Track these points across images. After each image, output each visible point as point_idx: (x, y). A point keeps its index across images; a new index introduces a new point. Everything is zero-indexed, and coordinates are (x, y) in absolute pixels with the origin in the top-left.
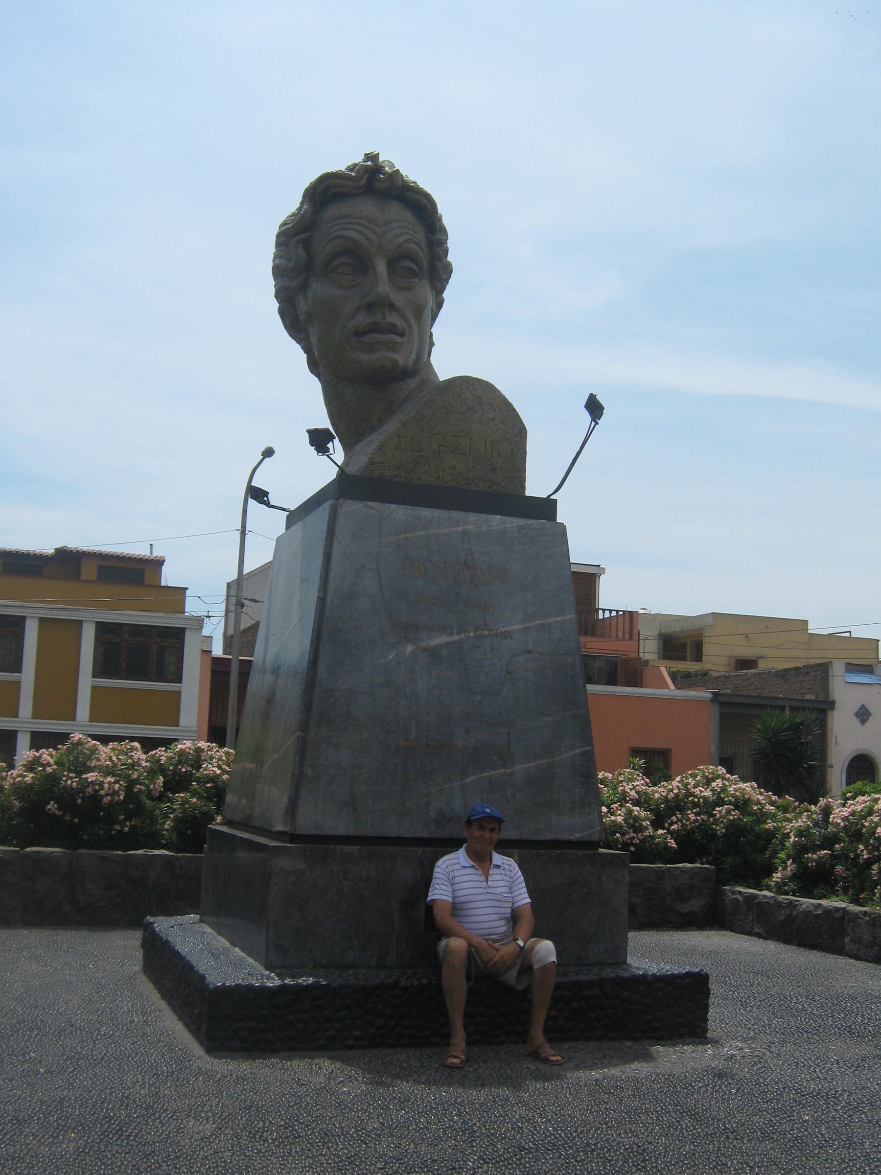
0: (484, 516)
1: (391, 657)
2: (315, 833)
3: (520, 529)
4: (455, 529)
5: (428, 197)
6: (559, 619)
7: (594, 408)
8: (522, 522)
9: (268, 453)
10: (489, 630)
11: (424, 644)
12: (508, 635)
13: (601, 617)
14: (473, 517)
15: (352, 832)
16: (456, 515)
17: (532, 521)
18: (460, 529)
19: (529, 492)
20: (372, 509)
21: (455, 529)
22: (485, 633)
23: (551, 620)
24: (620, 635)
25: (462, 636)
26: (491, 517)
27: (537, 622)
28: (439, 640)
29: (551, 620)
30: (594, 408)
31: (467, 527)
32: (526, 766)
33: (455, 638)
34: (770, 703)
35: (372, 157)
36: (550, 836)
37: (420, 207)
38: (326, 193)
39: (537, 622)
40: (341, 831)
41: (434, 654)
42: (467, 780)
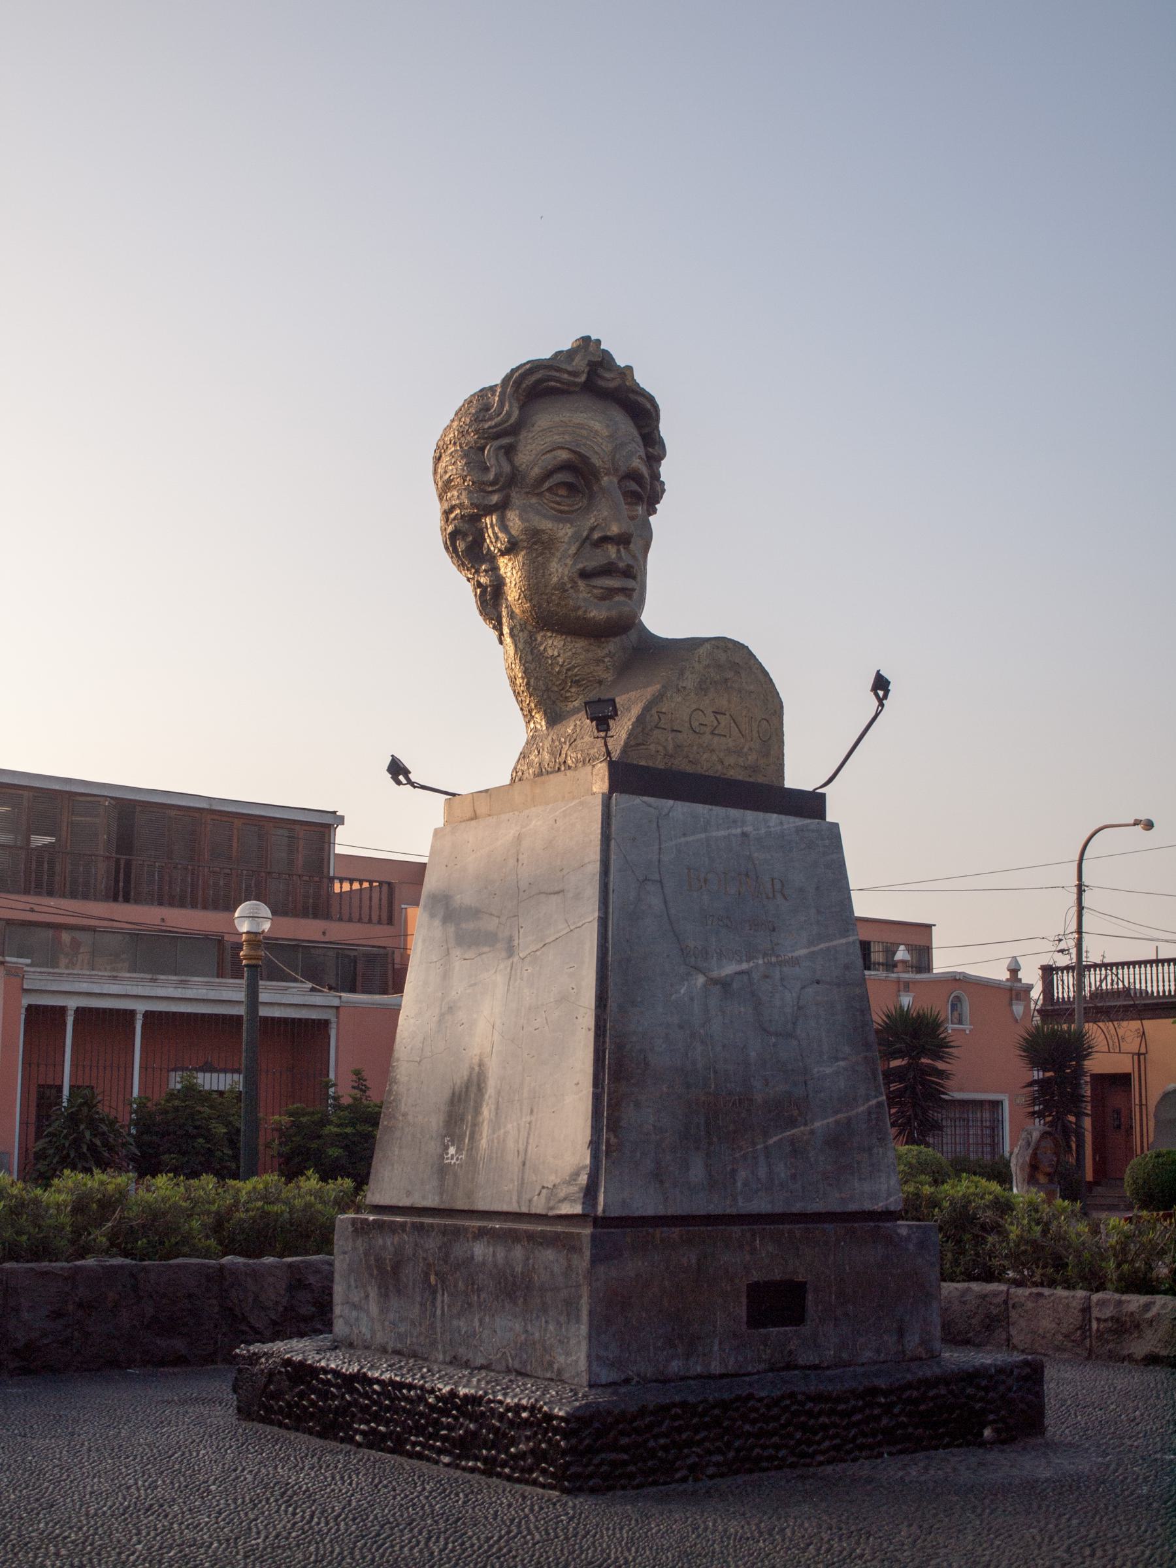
0: (761, 815)
1: (682, 991)
2: (839, 1210)
3: (799, 830)
4: (734, 831)
5: (651, 399)
6: (844, 941)
7: (881, 685)
8: (799, 822)
9: (1149, 825)
10: (778, 956)
11: (715, 974)
12: (795, 962)
13: (337, 889)
14: (750, 815)
15: (661, 1211)
16: (734, 813)
17: (809, 821)
18: (739, 831)
19: (788, 784)
20: (650, 806)
21: (734, 831)
22: (774, 959)
23: (835, 943)
24: (375, 918)
25: (751, 964)
26: (768, 815)
27: (822, 946)
28: (730, 969)
29: (835, 943)
30: (881, 685)
31: (745, 829)
32: (825, 1122)
33: (745, 966)
34: (1064, 1040)
35: (586, 340)
36: (852, 1207)
37: (641, 412)
38: (535, 385)
39: (822, 946)
40: (650, 1212)
41: (725, 985)
42: (771, 1142)
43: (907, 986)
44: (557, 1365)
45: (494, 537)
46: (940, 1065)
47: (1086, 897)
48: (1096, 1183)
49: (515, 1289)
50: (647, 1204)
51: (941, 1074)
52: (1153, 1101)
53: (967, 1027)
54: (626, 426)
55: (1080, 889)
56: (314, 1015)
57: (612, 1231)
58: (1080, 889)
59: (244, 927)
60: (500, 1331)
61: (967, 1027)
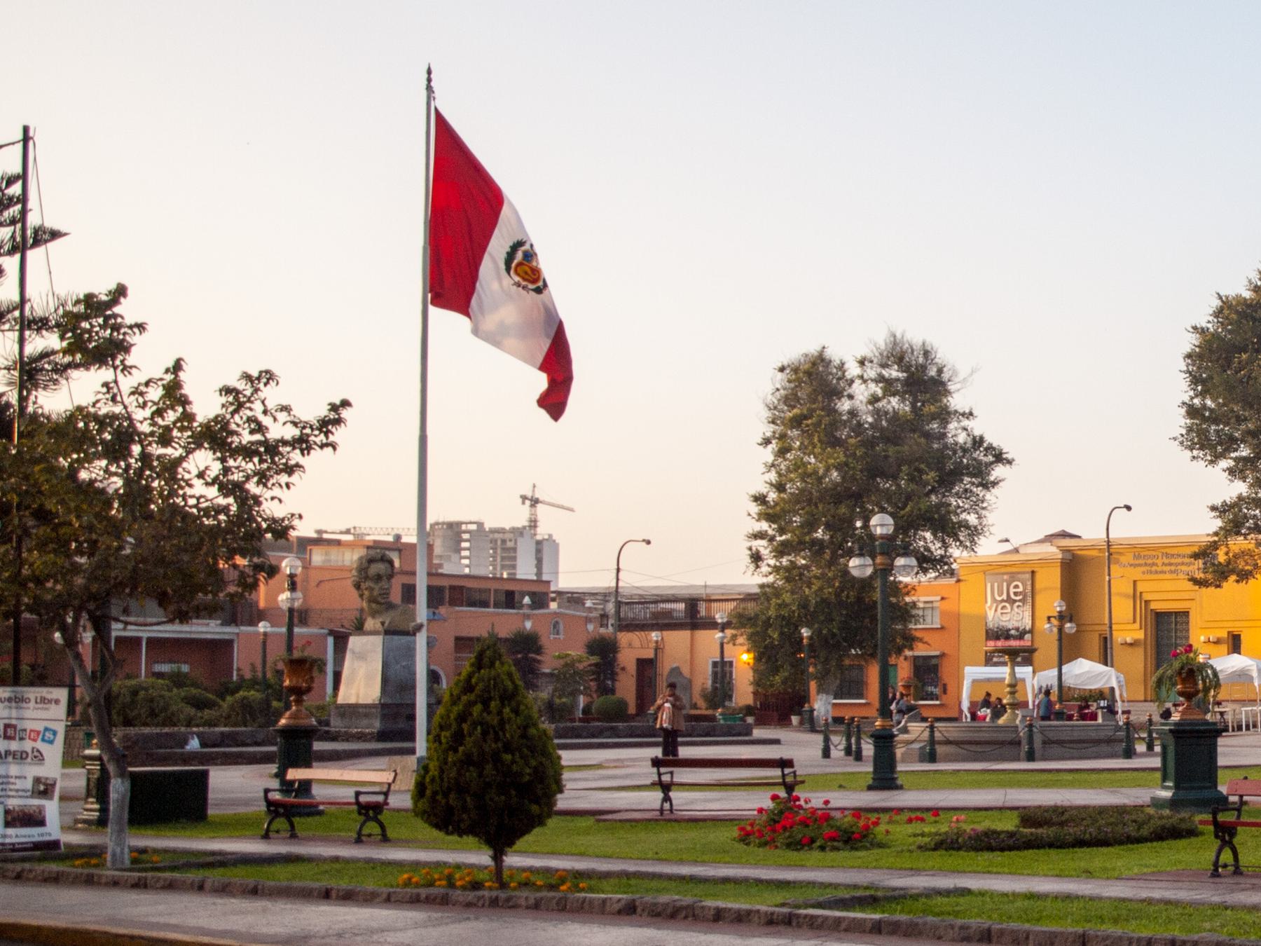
9: (648, 542)
43: (528, 617)
44: (376, 725)
45: (363, 586)
46: (539, 657)
47: (621, 574)
48: (637, 715)
49: (366, 715)
50: (389, 701)
51: (539, 662)
52: (665, 674)
53: (561, 637)
54: (387, 565)
55: (618, 570)
56: (227, 637)
57: (383, 706)
58: (618, 570)
59: (262, 630)
60: (365, 722)
61: (561, 637)
